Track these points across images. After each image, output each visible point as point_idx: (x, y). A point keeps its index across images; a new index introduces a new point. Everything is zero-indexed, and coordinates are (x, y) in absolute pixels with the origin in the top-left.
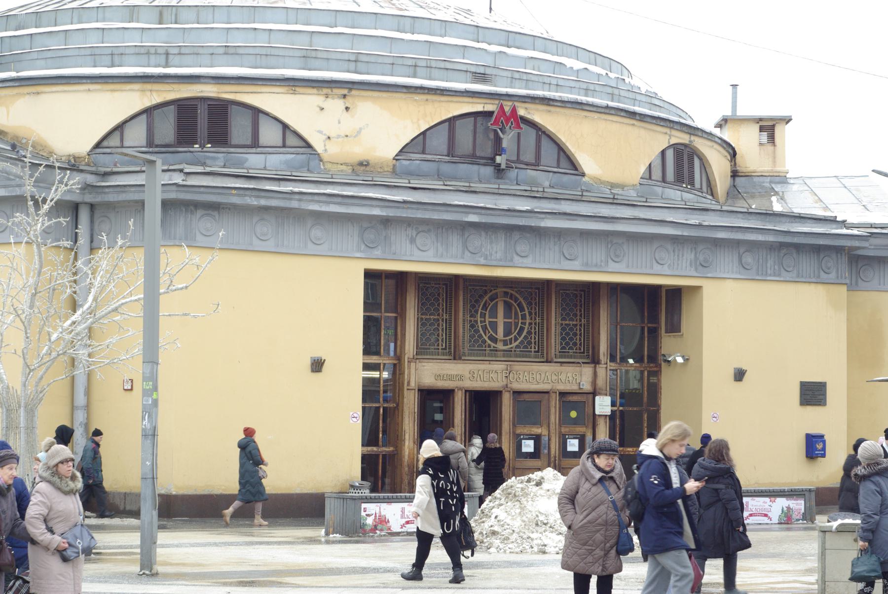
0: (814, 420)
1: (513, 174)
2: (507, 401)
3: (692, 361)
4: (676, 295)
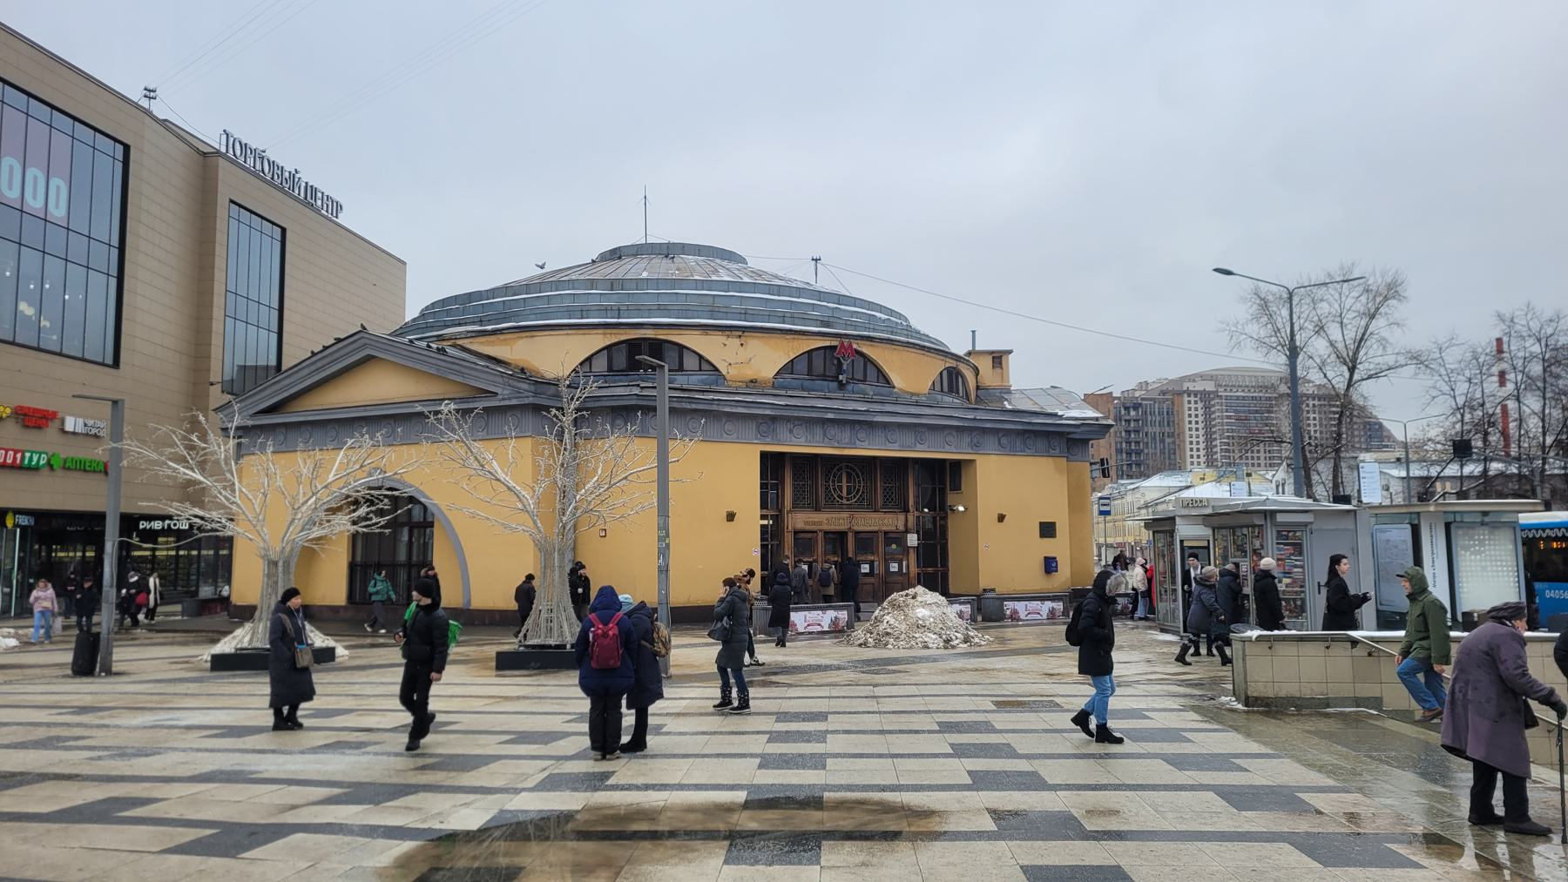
0: (1050, 547)
1: (850, 387)
2: (850, 537)
3: (971, 510)
4: (957, 466)
